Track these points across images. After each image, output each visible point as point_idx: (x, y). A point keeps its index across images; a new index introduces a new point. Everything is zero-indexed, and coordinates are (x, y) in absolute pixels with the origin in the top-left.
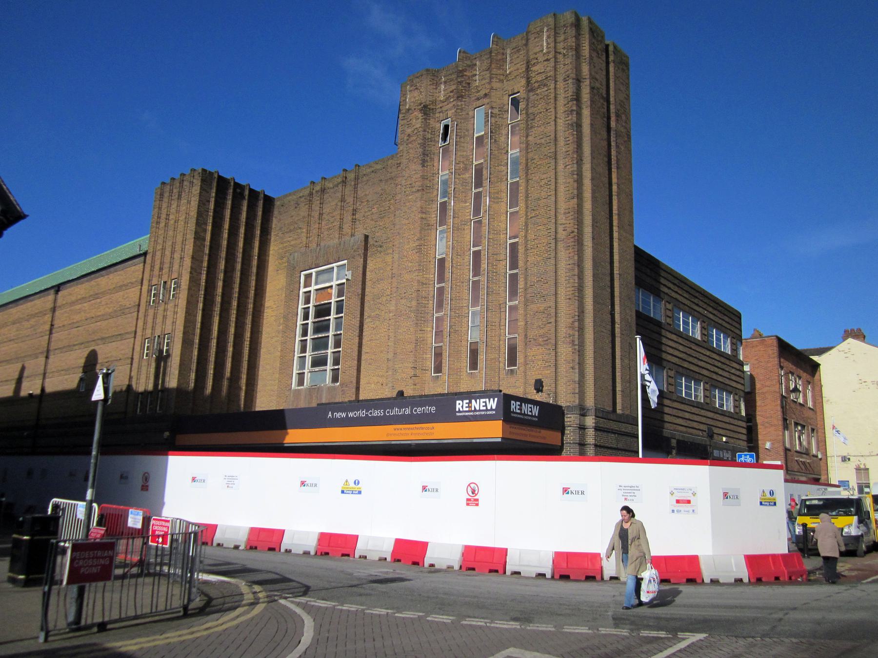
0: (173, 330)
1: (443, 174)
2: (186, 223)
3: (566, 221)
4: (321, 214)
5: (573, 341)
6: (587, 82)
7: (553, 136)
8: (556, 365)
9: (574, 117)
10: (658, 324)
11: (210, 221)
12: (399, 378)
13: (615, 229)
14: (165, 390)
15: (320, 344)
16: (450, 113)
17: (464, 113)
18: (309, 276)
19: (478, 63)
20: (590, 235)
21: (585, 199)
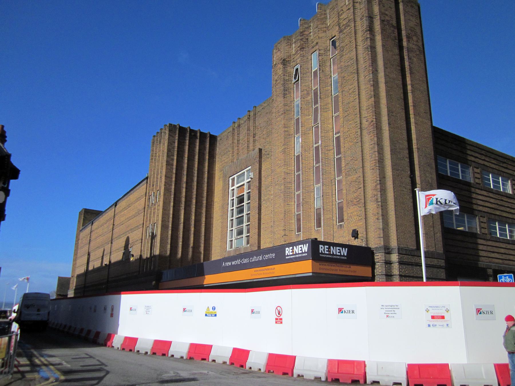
0: (158, 220)
1: (297, 101)
3: (368, 115)
4: (238, 141)
5: (377, 199)
6: (378, 17)
7: (355, 58)
8: (366, 218)
9: (368, 42)
10: (468, 184)
11: (176, 153)
12: (276, 237)
13: (412, 116)
14: (155, 256)
15: (240, 221)
16: (298, 60)
17: (305, 58)
18: (233, 180)
19: (312, 25)
20: (387, 122)
21: (381, 98)
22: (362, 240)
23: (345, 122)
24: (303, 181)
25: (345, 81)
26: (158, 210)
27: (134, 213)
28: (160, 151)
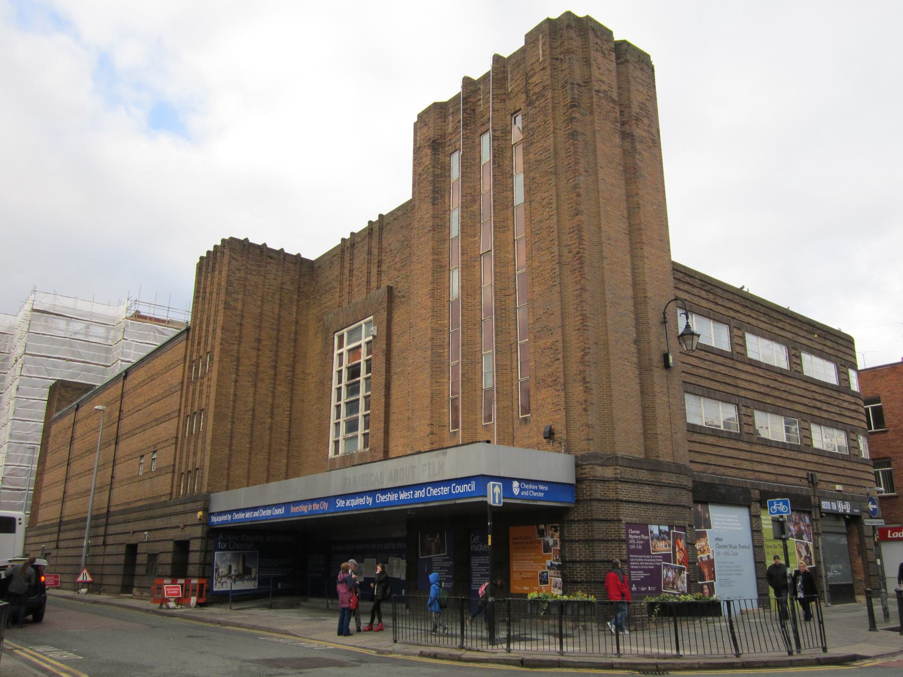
0: (207, 405)
2: (218, 294)
4: (351, 271)
12: (418, 437)
15: (352, 407)
19: (482, 87)
22: (560, 443)
23: (535, 252)
24: (463, 345)
25: (535, 185)
26: (209, 386)
27: (161, 391)
28: (212, 284)
